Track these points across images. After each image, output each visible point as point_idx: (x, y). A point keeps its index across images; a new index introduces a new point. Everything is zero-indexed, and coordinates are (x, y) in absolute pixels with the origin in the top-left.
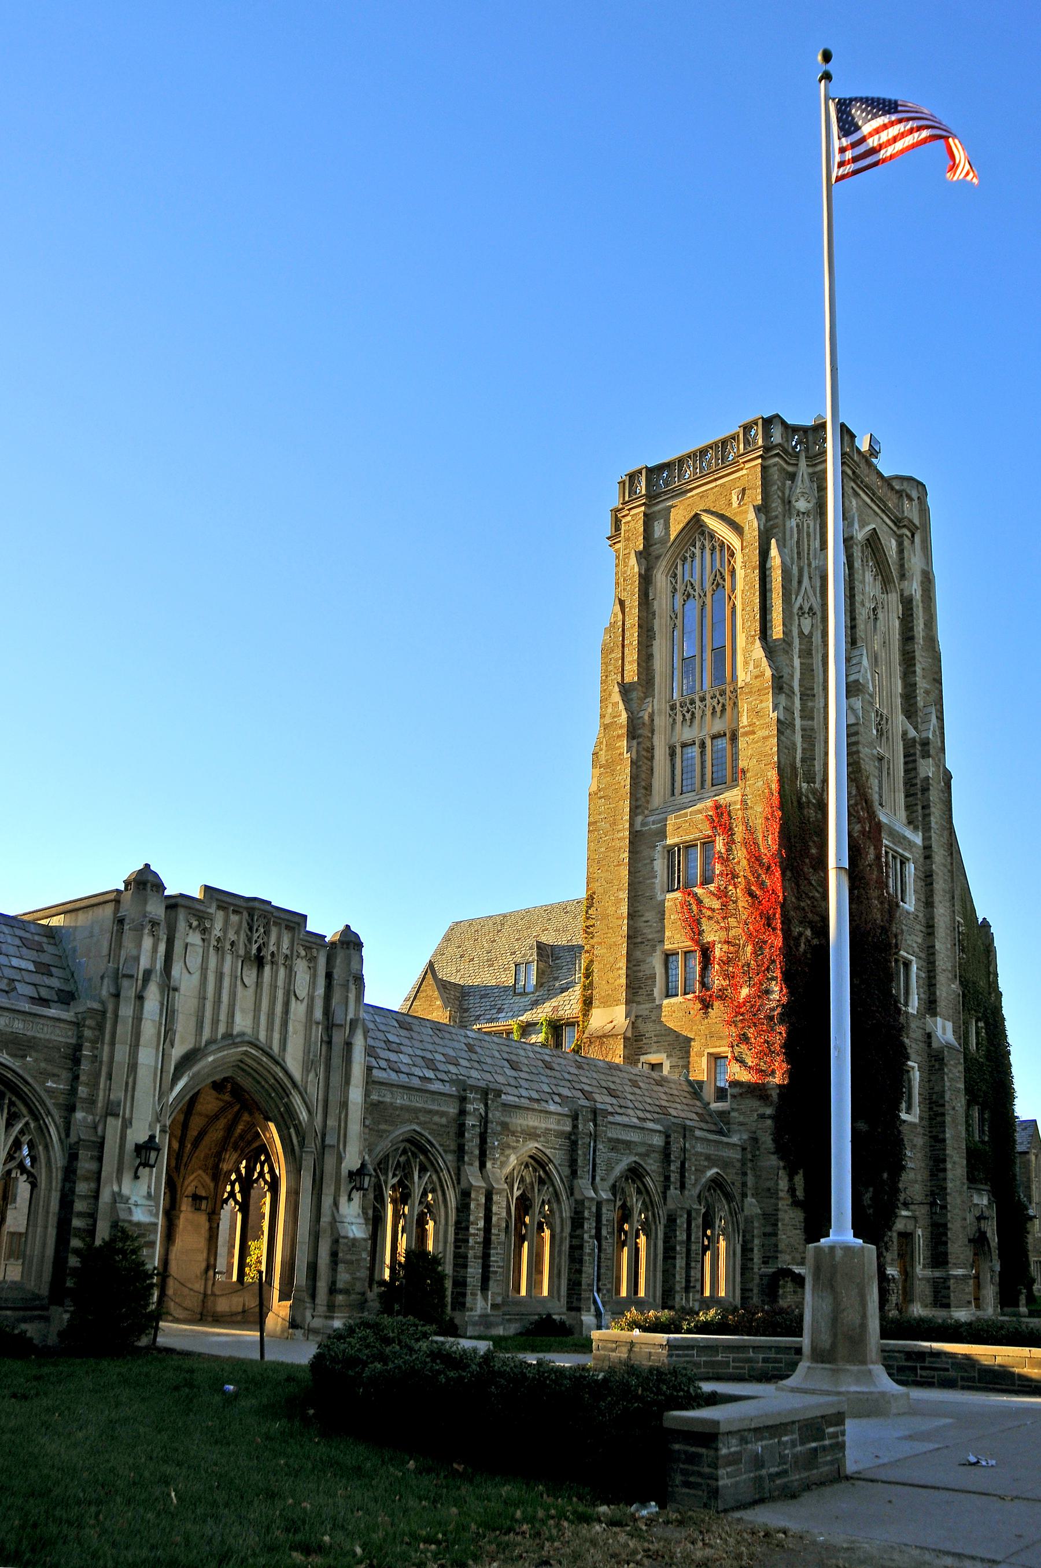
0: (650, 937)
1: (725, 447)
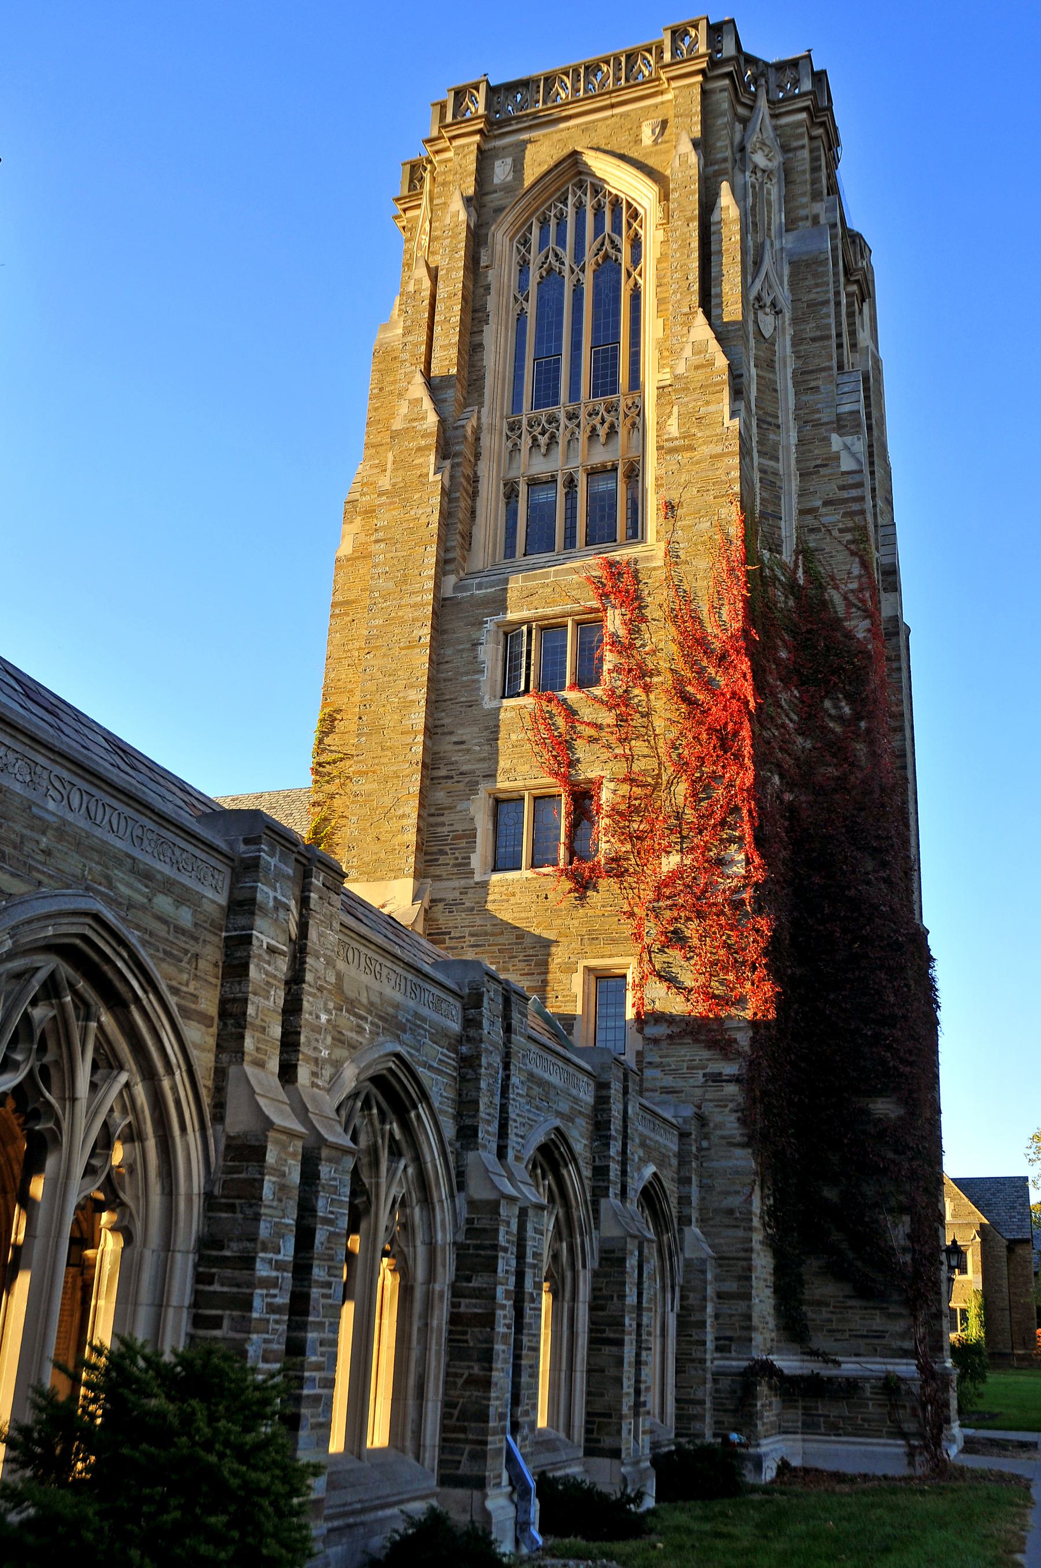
0: (465, 768)
1: (632, 62)
